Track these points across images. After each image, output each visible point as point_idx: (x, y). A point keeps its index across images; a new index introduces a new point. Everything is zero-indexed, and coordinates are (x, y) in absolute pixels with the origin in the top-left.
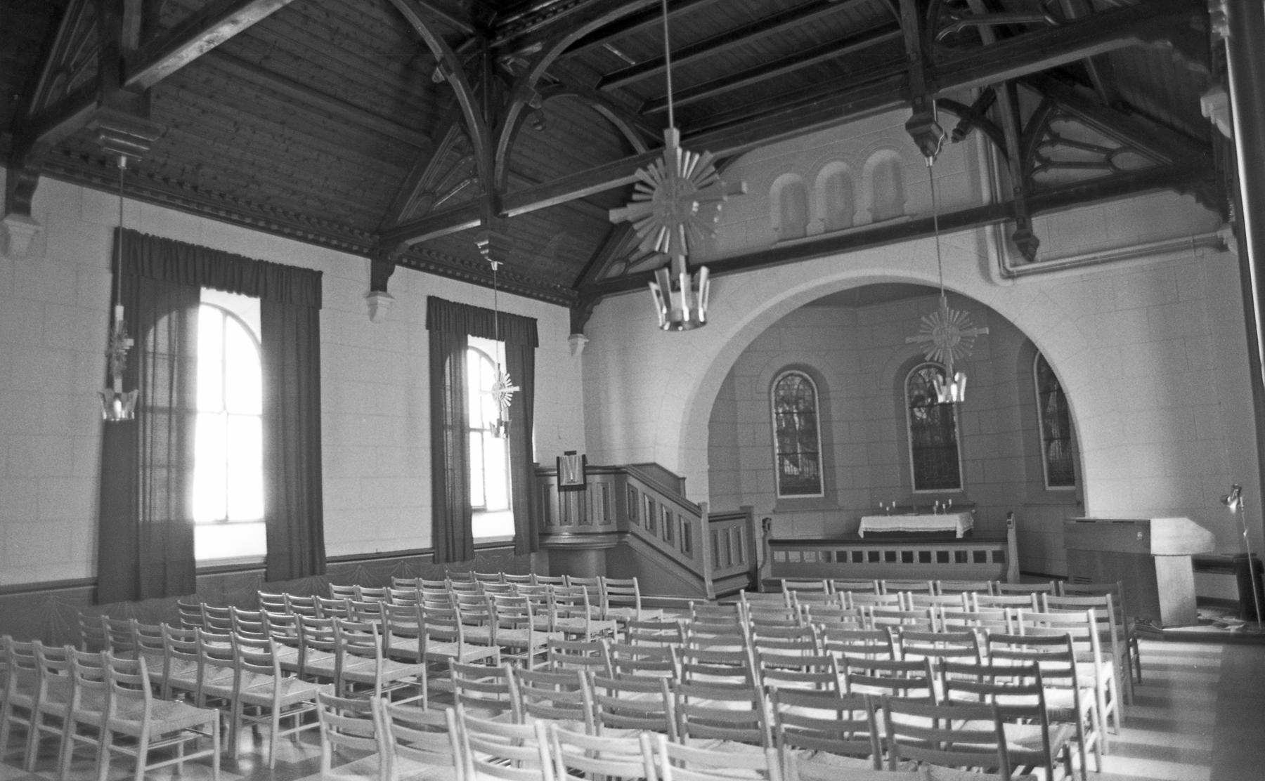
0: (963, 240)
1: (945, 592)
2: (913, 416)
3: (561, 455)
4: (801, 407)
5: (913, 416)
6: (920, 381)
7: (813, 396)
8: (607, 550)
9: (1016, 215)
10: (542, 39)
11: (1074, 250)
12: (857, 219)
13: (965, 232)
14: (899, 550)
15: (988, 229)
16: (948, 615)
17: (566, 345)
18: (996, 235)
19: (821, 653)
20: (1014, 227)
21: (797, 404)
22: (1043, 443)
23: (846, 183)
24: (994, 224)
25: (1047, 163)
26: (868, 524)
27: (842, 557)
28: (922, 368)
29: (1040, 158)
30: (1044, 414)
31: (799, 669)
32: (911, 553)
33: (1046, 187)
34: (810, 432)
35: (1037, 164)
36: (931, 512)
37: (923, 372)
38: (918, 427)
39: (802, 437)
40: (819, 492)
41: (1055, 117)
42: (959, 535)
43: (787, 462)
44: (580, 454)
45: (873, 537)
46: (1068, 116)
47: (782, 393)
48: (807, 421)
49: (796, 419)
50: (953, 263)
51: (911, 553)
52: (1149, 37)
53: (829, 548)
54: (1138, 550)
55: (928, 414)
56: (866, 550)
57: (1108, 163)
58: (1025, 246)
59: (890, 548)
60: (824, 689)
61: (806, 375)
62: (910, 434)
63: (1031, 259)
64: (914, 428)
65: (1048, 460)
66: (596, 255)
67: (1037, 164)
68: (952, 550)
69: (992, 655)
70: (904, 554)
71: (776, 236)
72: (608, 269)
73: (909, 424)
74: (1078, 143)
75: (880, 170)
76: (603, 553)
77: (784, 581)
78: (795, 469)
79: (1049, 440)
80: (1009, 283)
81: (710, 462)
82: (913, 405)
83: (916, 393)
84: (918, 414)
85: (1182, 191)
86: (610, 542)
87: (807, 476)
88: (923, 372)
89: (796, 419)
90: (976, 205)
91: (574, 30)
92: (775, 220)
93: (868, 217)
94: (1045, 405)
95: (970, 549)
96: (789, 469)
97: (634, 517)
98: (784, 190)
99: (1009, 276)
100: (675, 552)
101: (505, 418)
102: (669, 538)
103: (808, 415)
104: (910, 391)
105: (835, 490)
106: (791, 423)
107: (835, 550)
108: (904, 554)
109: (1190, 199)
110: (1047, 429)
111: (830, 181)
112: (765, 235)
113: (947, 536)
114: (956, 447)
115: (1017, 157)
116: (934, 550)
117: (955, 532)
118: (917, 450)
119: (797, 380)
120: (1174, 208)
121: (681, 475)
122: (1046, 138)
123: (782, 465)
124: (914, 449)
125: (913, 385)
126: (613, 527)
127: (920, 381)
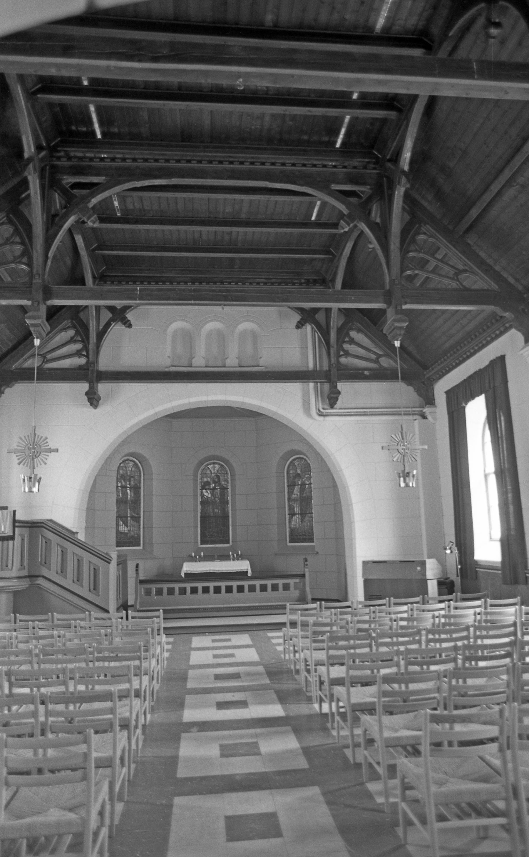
0: (294, 389)
1: (396, 604)
2: (202, 495)
3: (11, 509)
4: (132, 483)
5: (202, 495)
6: (208, 472)
7: (140, 476)
8: (16, 593)
9: (328, 379)
10: (106, 175)
11: (354, 405)
12: (195, 362)
13: (296, 384)
14: (211, 585)
15: (311, 385)
16: (359, 622)
17: (310, 421)
18: (316, 388)
19: (423, 647)
20: (327, 386)
21: (130, 481)
22: (287, 516)
23: (221, 338)
24: (314, 382)
25: (347, 354)
26: (188, 567)
27: (159, 592)
28: (210, 464)
29: (344, 350)
30: (289, 499)
31: (434, 657)
32: (185, 589)
33: (346, 367)
34: (136, 502)
35: (342, 353)
36: (230, 560)
37: (210, 467)
38: (205, 502)
39: (129, 506)
40: (139, 545)
41: (351, 329)
42: (249, 575)
43: (121, 523)
44: (11, 509)
45: (191, 577)
46: (359, 331)
47: (121, 472)
48: (135, 494)
49: (129, 491)
50: (286, 403)
51: (185, 589)
52: (505, 310)
53: (148, 586)
54: (419, 577)
55: (212, 494)
56: (188, 586)
57: (376, 361)
58: (332, 398)
59: (229, 583)
60: (467, 665)
61: (221, 463)
62: (199, 507)
63: (332, 407)
64: (202, 503)
65: (290, 527)
66: (14, 348)
67: (342, 353)
68: (246, 584)
69: (476, 638)
70: (168, 589)
71: (168, 362)
72: (25, 360)
73: (199, 499)
74: (360, 347)
75: (243, 334)
76: (11, 596)
77: (288, 604)
78: (126, 529)
79: (292, 514)
80: (321, 418)
81: (86, 523)
82: (203, 488)
83: (205, 480)
84: (206, 494)
85: (409, 384)
86: (23, 584)
87: (132, 533)
88: (210, 467)
89: (129, 491)
90: (304, 369)
91: (138, 180)
92: (168, 351)
93: (236, 362)
94: (290, 493)
95: (258, 583)
96: (123, 528)
97: (46, 563)
98: (175, 332)
99: (321, 414)
100: (84, 592)
101: (340, 473)
102: (79, 580)
103: (136, 489)
104: (202, 478)
105: (151, 544)
106: (125, 494)
107: (154, 587)
108: (168, 589)
109: (411, 389)
110: (291, 508)
111: (209, 334)
112: (161, 359)
113: (241, 575)
114: (228, 516)
115: (335, 346)
116: (235, 584)
117: (247, 572)
118: (204, 518)
119: (132, 464)
120: (403, 392)
121: (74, 530)
122: (347, 339)
123: (118, 525)
124: (201, 517)
125: (204, 475)
126: (25, 573)
127: (208, 472)
